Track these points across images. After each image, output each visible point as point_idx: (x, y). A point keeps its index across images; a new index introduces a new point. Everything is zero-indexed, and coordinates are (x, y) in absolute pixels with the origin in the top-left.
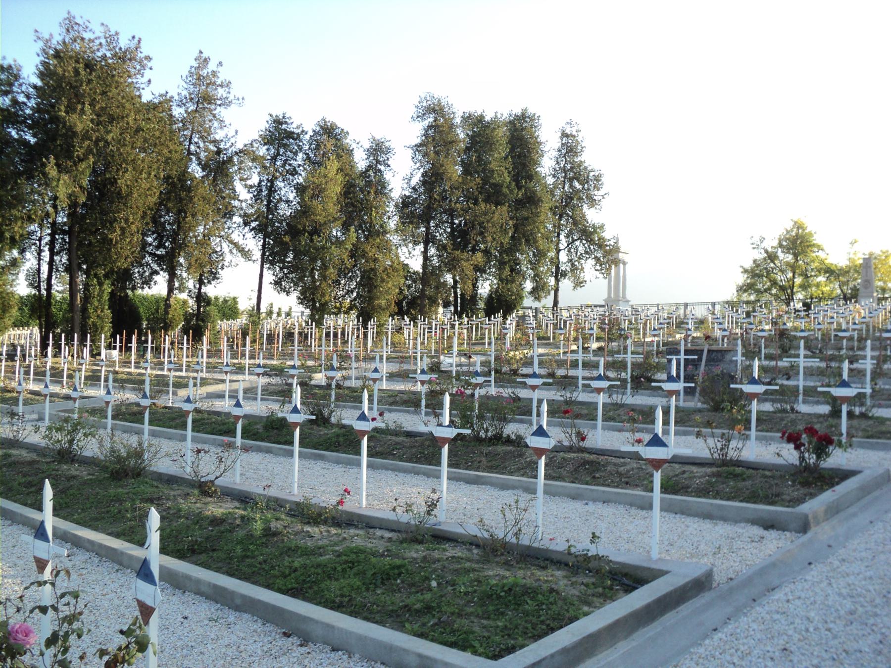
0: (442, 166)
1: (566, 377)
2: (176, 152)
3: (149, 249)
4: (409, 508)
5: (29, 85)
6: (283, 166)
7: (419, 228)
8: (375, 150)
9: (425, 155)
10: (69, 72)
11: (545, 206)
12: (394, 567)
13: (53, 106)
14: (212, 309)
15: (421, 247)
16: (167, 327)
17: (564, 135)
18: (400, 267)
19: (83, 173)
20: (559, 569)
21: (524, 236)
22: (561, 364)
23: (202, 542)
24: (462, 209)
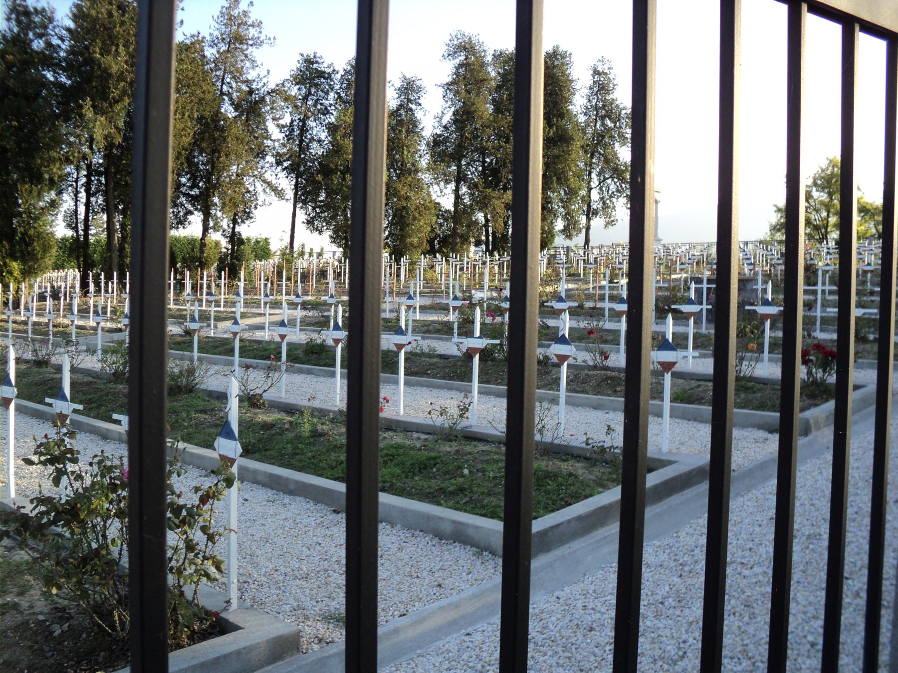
0: (473, 104)
1: (594, 308)
2: (209, 92)
3: (183, 189)
4: (443, 412)
5: (62, 27)
6: (315, 105)
7: (450, 167)
8: (406, 89)
9: (457, 93)
10: (102, 14)
11: (577, 144)
12: (430, 459)
13: (87, 48)
14: (247, 249)
15: (452, 186)
16: (203, 265)
17: (596, 72)
18: (432, 205)
19: (118, 114)
20: (578, 462)
21: (555, 175)
22: (589, 297)
23: (254, 443)
24: (493, 148)
